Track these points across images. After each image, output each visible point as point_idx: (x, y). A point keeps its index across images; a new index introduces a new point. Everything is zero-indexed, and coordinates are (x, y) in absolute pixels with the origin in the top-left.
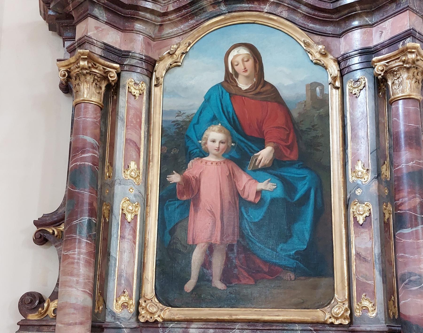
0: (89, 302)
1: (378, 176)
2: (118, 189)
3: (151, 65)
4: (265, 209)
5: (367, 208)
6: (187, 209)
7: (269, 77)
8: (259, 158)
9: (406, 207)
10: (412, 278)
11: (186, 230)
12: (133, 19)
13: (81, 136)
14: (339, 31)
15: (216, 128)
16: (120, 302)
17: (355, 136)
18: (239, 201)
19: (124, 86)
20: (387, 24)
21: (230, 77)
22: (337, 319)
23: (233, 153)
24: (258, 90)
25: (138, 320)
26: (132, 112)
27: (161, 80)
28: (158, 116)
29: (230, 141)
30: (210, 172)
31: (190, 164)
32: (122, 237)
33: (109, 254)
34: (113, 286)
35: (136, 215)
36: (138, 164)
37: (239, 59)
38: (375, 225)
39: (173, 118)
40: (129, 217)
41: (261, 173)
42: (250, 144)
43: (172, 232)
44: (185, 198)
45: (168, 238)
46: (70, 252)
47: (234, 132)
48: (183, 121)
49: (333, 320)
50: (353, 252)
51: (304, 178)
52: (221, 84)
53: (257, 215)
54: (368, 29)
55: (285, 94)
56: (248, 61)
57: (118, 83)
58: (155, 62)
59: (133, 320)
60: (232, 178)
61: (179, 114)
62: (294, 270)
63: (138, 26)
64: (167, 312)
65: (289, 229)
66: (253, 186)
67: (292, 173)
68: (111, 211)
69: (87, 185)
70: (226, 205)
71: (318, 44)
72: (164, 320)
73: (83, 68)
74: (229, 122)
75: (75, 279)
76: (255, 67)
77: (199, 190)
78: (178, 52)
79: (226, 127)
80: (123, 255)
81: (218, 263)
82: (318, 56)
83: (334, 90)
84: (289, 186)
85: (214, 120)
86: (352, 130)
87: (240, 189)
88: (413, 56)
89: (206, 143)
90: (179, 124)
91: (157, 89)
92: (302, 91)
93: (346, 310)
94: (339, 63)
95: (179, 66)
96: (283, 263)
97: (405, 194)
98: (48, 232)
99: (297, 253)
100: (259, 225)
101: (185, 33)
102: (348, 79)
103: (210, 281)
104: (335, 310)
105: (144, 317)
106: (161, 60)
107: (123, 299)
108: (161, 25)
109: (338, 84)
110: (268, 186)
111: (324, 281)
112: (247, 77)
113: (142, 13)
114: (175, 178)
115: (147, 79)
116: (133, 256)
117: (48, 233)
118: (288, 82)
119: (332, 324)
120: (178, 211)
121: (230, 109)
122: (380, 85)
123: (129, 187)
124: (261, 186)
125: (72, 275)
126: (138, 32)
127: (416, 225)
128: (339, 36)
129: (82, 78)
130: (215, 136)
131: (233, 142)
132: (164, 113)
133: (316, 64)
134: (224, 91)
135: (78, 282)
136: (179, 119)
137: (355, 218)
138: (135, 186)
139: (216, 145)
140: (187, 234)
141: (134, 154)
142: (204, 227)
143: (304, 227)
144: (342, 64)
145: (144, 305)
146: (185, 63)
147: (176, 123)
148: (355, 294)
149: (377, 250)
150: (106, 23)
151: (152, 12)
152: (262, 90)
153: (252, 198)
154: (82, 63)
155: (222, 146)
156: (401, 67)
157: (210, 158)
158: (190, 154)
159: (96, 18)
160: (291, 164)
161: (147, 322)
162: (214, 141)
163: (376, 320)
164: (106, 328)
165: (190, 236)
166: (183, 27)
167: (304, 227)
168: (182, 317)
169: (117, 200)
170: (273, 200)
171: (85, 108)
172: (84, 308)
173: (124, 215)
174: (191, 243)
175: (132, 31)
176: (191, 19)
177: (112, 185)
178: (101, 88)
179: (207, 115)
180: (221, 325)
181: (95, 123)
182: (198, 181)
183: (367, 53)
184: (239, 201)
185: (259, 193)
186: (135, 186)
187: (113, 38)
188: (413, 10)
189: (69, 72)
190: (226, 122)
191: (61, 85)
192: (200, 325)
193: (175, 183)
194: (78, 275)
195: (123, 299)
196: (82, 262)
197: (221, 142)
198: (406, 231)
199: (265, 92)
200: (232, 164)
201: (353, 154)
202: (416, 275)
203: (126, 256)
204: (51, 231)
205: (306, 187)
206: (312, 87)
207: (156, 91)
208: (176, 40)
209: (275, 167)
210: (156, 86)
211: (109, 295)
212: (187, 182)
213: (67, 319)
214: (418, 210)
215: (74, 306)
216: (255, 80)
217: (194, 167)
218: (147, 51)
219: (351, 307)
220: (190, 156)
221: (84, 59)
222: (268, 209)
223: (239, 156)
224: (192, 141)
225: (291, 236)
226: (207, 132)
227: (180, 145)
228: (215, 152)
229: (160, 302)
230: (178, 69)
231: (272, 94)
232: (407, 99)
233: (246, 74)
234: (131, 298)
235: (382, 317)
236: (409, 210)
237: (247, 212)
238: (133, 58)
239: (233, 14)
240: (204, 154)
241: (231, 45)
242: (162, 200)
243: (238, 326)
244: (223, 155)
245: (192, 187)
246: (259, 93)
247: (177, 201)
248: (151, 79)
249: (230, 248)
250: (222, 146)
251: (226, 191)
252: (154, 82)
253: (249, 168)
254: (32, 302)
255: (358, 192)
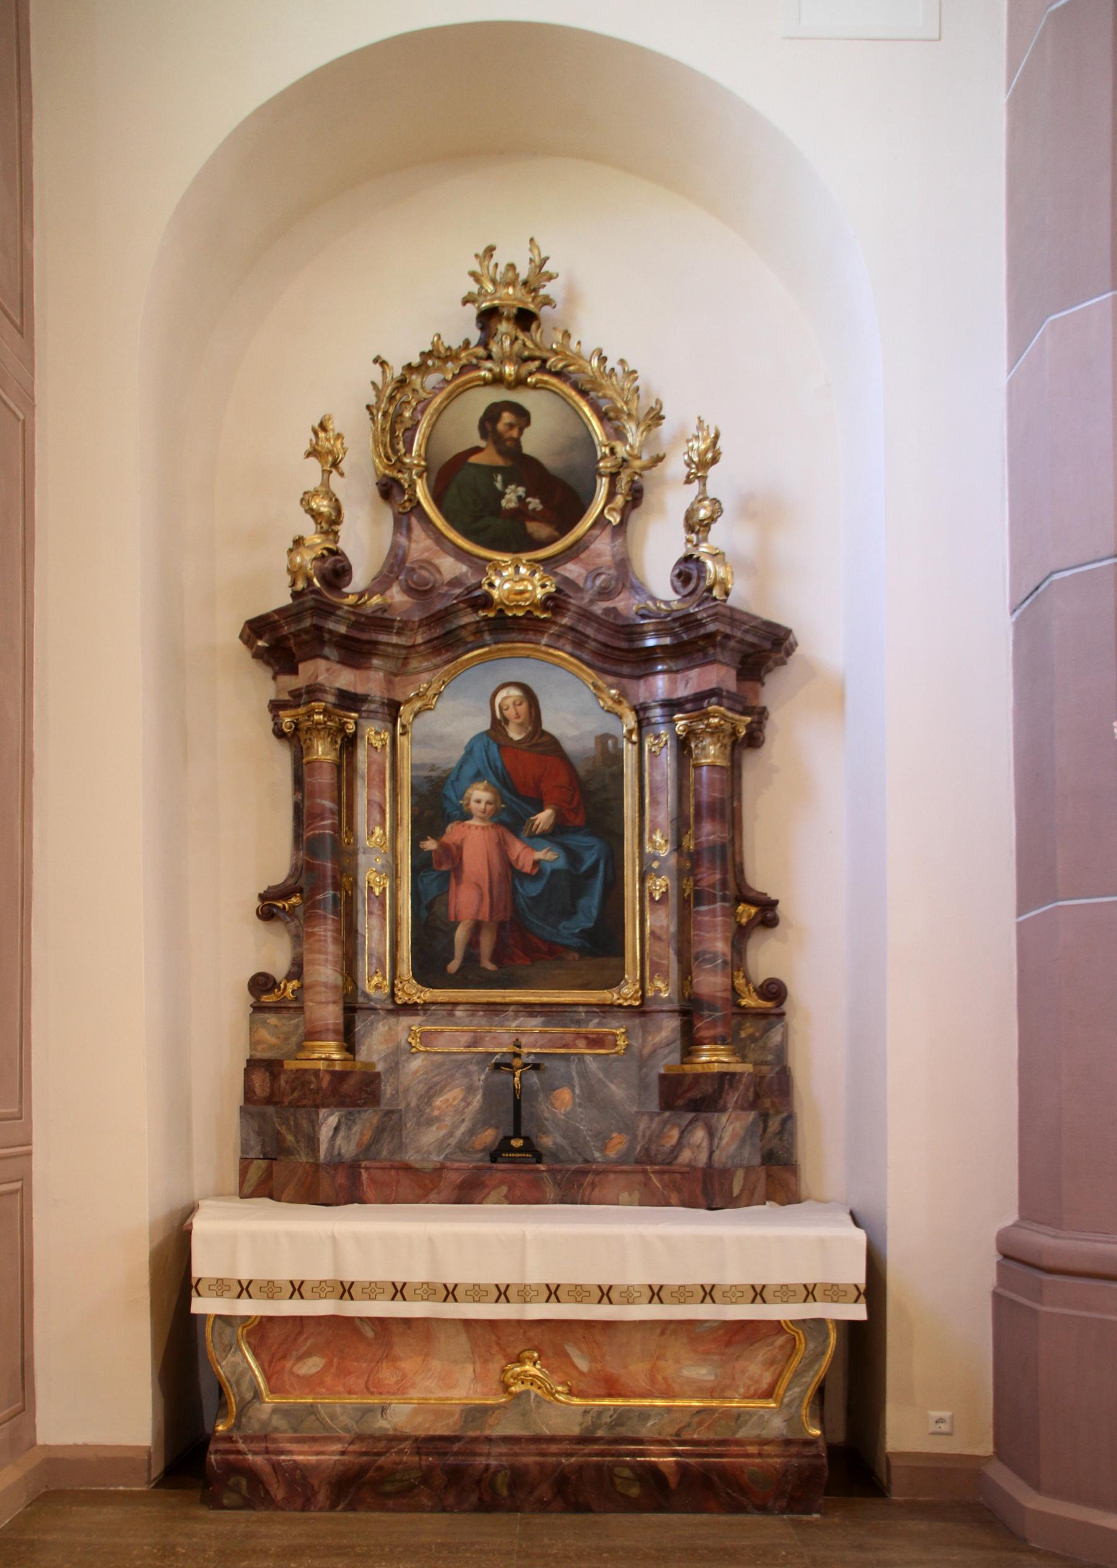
0: (340, 981)
1: (678, 847)
2: (362, 859)
3: (393, 709)
4: (543, 882)
5: (664, 884)
6: (447, 881)
7: (549, 724)
8: (537, 822)
9: (704, 883)
10: (707, 956)
11: (447, 905)
12: (371, 654)
13: (319, 801)
14: (638, 672)
15: (481, 786)
16: (374, 983)
17: (654, 802)
18: (511, 872)
19: (363, 737)
20: (694, 673)
21: (498, 725)
22: (626, 1000)
23: (504, 817)
24: (534, 741)
25: (394, 1002)
26: (374, 767)
27: (409, 728)
28: (405, 771)
29: (499, 802)
30: (474, 839)
31: (449, 829)
32: (370, 913)
33: (356, 931)
34: (364, 966)
35: (384, 889)
36: (384, 828)
37: (509, 702)
38: (673, 901)
39: (426, 773)
40: (377, 891)
41: (539, 840)
42: (525, 806)
43: (430, 907)
44: (444, 868)
45: (424, 914)
46: (316, 929)
47: (505, 792)
48: (439, 777)
49: (621, 1001)
50: (648, 931)
51: (591, 847)
52: (487, 733)
53: (534, 889)
54: (673, 676)
55: (568, 746)
56: (520, 704)
57: (355, 735)
58: (399, 704)
59: (389, 1001)
60: (502, 847)
61: (433, 768)
62: (580, 950)
63: (375, 662)
64: (428, 994)
65: (574, 905)
66: (528, 856)
67: (577, 841)
68: (355, 883)
69: (329, 853)
70: (496, 877)
71: (611, 687)
72: (425, 1003)
73: (318, 723)
74: (498, 778)
75: (323, 957)
76: (530, 713)
77: (461, 859)
78: (430, 693)
79: (494, 786)
80: (373, 933)
81: (487, 943)
82: (610, 703)
83: (630, 746)
84: (573, 856)
85: (478, 777)
86: (651, 794)
87: (513, 858)
88: (716, 720)
89: (468, 804)
90: (432, 781)
91: (404, 738)
92: (590, 744)
93: (636, 992)
94: (637, 712)
95: (430, 709)
96: (568, 942)
97: (703, 869)
98: (270, 907)
99: (582, 931)
100: (536, 900)
101: (437, 667)
102: (648, 733)
103: (479, 961)
104: (625, 990)
105: (402, 997)
106: (409, 701)
107: (376, 980)
108: (406, 658)
109: (634, 738)
110: (547, 855)
111: (613, 961)
112: (521, 725)
113: (381, 647)
114: (430, 845)
115: (390, 726)
116: (385, 932)
117: (278, 907)
118: (572, 732)
119: (620, 1006)
120: (435, 883)
121: (499, 764)
122: (683, 746)
123: (374, 857)
124: (538, 855)
125: (320, 952)
126: (377, 669)
127: (714, 902)
128: (639, 678)
129: (315, 733)
130: (479, 796)
131: (503, 802)
132: (414, 767)
133: (608, 711)
134: (491, 742)
135: (327, 960)
136: (434, 774)
137: (651, 894)
138: (381, 852)
139: (482, 806)
140: (447, 910)
141: (378, 817)
142: (468, 902)
143: (591, 903)
144: (641, 714)
145: (400, 986)
146: (439, 705)
147: (429, 779)
148: (647, 974)
149: (673, 929)
150: (339, 662)
151: (395, 646)
152: (540, 741)
153: (528, 869)
154: (316, 717)
155: (489, 807)
156: (703, 731)
157: (474, 822)
158: (448, 816)
159: (327, 658)
160: (576, 830)
161: (405, 1004)
162: (479, 801)
163: (669, 1000)
164: (361, 1009)
165: (452, 912)
166: (437, 660)
167: (591, 903)
168: (446, 1000)
169: (361, 871)
170: (554, 872)
171: (321, 767)
172: (335, 987)
173: (371, 889)
174: (453, 920)
175: (369, 668)
176: (447, 651)
177: (354, 854)
178: (336, 742)
179: (469, 770)
180: (492, 1008)
181: (332, 784)
182: (460, 849)
183: (672, 706)
184: (511, 872)
185: (536, 863)
186: (381, 852)
187: (346, 679)
188: (720, 662)
189: (296, 724)
190: (493, 779)
191: (274, 731)
192: (467, 1007)
193: (431, 851)
194: (326, 953)
195: (376, 980)
196: (330, 940)
197: (488, 803)
198: (703, 908)
199: (542, 744)
200: (502, 829)
201: (651, 821)
202: (710, 953)
203: (376, 933)
204: (280, 905)
205: (594, 858)
206: (603, 739)
207: (403, 742)
208: (425, 676)
209: (554, 834)
210: (401, 734)
211: (359, 975)
212: (445, 848)
213: (319, 998)
214: (718, 887)
215: (325, 985)
216: (530, 728)
217: (453, 833)
218: (389, 691)
219: (642, 987)
220: (448, 819)
221: (319, 713)
222: (548, 881)
223: (511, 819)
224: (451, 801)
225: (575, 913)
226: (469, 791)
227: (435, 806)
228: (480, 814)
229: (419, 983)
230: (429, 713)
231: (553, 745)
232: (712, 766)
233: (519, 721)
234: (384, 978)
235: (675, 997)
236: (708, 886)
237: (522, 885)
238: (373, 702)
239: (500, 646)
240: (468, 816)
241: (498, 684)
242: (415, 871)
243: (512, 1008)
244: (491, 818)
245: (454, 855)
246: (536, 745)
247: (434, 874)
248: (395, 725)
249: (501, 926)
250: (489, 807)
251: (496, 860)
252: (399, 730)
253: (524, 835)
254: (265, 984)
255: (655, 865)
